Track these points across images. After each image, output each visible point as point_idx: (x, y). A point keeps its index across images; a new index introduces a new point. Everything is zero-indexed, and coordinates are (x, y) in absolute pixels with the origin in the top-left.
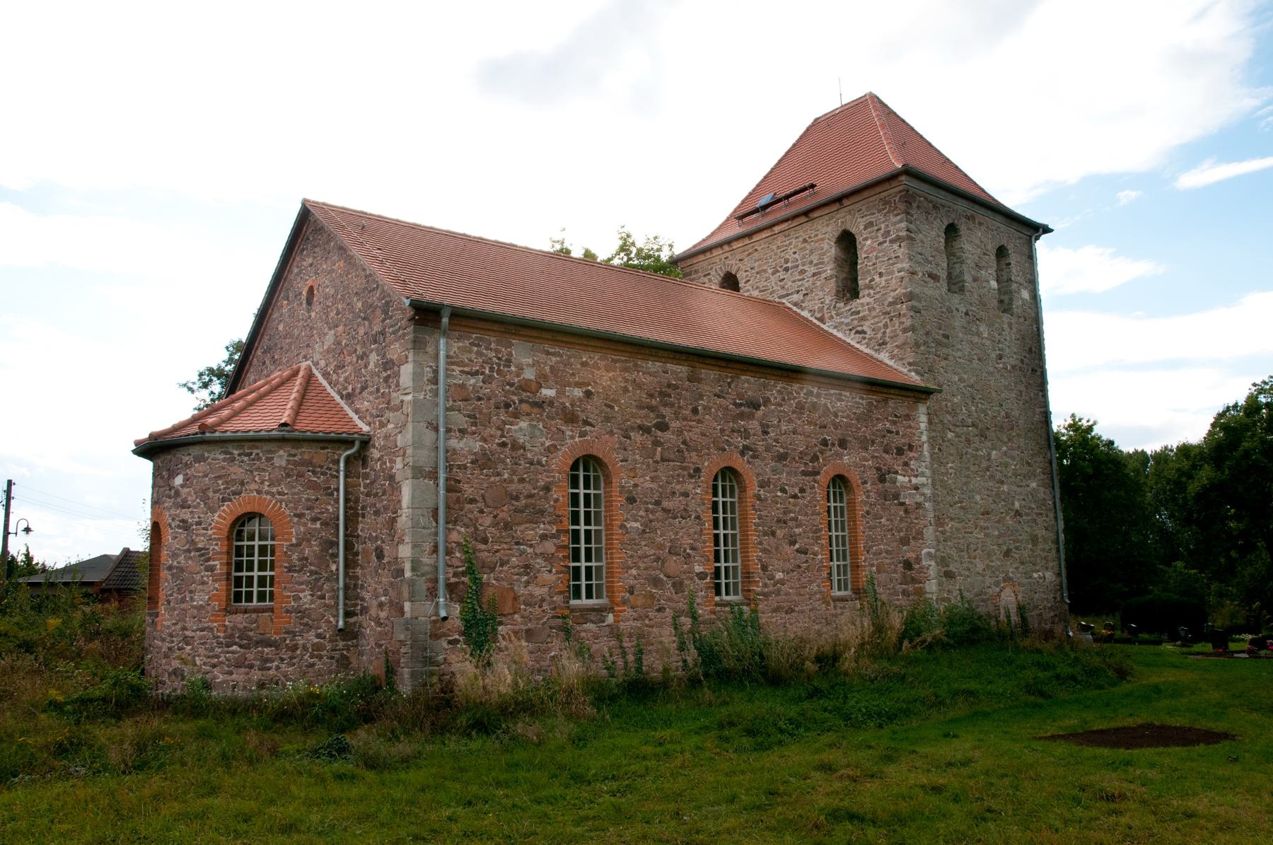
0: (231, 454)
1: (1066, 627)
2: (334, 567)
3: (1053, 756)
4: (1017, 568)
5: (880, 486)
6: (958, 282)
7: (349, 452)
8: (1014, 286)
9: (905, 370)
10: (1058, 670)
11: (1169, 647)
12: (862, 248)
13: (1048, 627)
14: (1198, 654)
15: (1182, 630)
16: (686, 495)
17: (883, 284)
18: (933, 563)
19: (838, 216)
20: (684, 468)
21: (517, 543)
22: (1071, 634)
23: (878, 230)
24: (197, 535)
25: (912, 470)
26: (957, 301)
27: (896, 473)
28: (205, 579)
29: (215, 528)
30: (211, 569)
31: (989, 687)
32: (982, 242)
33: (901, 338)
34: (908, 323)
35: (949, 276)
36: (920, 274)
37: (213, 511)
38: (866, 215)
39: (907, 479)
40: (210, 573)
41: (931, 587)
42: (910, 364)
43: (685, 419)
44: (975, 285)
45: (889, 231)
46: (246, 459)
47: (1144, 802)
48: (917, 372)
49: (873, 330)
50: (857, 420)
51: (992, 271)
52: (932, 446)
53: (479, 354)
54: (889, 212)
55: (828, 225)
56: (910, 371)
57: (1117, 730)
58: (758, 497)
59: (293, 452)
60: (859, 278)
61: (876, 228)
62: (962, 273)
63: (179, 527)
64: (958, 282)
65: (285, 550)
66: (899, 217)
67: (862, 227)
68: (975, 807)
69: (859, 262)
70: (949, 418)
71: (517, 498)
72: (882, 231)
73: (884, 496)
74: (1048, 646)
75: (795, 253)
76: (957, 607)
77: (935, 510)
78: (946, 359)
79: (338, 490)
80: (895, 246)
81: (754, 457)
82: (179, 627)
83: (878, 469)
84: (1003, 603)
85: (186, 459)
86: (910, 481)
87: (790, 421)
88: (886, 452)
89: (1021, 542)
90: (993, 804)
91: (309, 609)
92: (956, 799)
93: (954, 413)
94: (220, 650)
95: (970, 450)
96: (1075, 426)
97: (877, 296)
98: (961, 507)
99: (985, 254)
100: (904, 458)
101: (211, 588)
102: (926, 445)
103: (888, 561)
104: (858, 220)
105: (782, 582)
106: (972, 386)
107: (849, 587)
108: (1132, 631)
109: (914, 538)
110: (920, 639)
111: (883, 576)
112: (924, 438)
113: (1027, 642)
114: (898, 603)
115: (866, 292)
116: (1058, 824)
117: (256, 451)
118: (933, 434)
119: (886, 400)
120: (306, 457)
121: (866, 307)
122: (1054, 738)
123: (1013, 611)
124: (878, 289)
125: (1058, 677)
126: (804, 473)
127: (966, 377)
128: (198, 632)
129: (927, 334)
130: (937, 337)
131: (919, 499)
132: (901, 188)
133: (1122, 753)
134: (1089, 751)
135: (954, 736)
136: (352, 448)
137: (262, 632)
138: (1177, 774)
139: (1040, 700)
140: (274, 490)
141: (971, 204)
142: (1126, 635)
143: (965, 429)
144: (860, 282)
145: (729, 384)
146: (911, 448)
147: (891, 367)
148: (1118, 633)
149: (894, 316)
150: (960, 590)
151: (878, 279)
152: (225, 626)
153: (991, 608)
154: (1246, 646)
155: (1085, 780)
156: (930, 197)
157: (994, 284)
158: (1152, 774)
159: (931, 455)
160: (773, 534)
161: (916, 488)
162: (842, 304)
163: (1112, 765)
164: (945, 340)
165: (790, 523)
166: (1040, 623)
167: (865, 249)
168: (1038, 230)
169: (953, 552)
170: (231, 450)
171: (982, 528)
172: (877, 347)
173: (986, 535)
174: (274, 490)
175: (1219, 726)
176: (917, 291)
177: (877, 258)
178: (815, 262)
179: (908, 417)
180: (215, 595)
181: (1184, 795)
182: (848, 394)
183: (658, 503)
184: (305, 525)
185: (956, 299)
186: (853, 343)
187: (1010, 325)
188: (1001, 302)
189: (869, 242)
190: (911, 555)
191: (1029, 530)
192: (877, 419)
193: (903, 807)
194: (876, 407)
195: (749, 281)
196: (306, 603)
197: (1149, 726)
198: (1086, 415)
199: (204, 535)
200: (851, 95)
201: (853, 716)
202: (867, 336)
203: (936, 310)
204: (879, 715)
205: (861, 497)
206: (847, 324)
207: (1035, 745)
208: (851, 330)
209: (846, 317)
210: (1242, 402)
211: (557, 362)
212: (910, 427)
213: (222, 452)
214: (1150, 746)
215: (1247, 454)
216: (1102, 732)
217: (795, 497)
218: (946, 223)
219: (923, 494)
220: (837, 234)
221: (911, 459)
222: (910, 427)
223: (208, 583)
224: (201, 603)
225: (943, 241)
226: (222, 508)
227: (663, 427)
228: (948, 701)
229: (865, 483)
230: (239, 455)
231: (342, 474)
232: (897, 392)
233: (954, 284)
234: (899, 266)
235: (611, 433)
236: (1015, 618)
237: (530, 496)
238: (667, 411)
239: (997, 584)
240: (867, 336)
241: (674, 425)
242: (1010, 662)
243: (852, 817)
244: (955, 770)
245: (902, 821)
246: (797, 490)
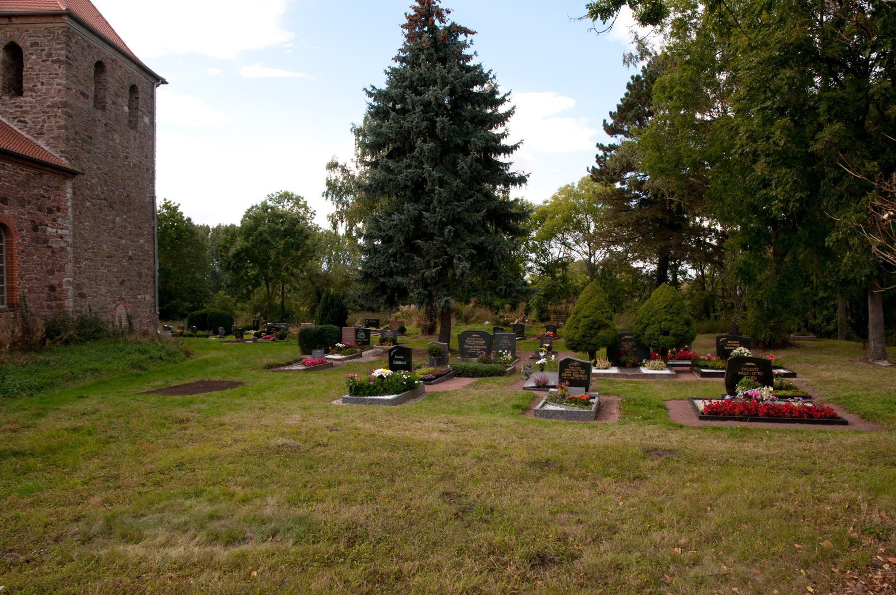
1: (156, 328)
3: (149, 403)
4: (128, 292)
5: (34, 233)
6: (102, 103)
8: (140, 113)
9: (57, 156)
10: (151, 354)
11: (213, 338)
12: (27, 60)
13: (145, 328)
14: (228, 342)
15: (221, 329)
17: (44, 90)
18: (71, 288)
19: (6, 29)
22: (159, 332)
25: (59, 225)
26: (100, 115)
27: (47, 225)
31: (108, 366)
32: (120, 79)
33: (56, 132)
34: (62, 123)
35: (96, 97)
36: (74, 91)
38: (33, 36)
39: (54, 230)
41: (69, 303)
42: (61, 152)
44: (113, 107)
45: (51, 54)
47: (199, 421)
48: (67, 158)
49: (34, 122)
50: (17, 185)
51: (126, 100)
52: (75, 210)
54: (52, 39)
56: (61, 156)
57: (185, 385)
60: (24, 81)
61: (41, 48)
62: (105, 97)
64: (102, 103)
66: (60, 46)
67: (28, 44)
68: (103, 436)
70: (88, 192)
72: (45, 52)
73: (36, 240)
74: (145, 340)
76: (86, 316)
77: (74, 253)
78: (89, 153)
80: (56, 66)
83: (33, 222)
84: (117, 314)
86: (57, 232)
88: (40, 210)
89: (132, 276)
90: (114, 433)
92: (90, 434)
93: (91, 189)
95: (101, 215)
96: (166, 206)
97: (38, 98)
98: (93, 252)
99: (122, 88)
102: (70, 209)
103: (37, 285)
106: (106, 174)
107: (5, 302)
108: (193, 330)
109: (58, 270)
110: (59, 337)
111: (33, 296)
112: (69, 204)
113: (132, 337)
114: (43, 313)
115: (29, 93)
116: (153, 439)
118: (76, 202)
119: (41, 175)
121: (29, 105)
122: (148, 393)
123: (124, 319)
124: (39, 94)
125: (151, 358)
127: (102, 167)
129: (76, 133)
130: (83, 136)
131: (63, 244)
133: (188, 397)
134: (169, 398)
135: (86, 397)
138: (216, 405)
139: (139, 372)
141: (116, 52)
142: (190, 332)
143: (99, 201)
144: (24, 85)
146: (59, 209)
147: (46, 151)
148: (186, 332)
150: (89, 305)
153: (110, 317)
154: (252, 337)
155: (168, 413)
156: (86, 38)
157: (126, 109)
158: (203, 406)
159: (74, 216)
161: (61, 237)
162: (7, 98)
163: (183, 405)
164: (89, 140)
166: (140, 326)
167: (30, 61)
168: (159, 81)
169: (86, 281)
171: (107, 266)
172: (36, 135)
173: (109, 271)
175: (237, 379)
176: (71, 102)
179: (58, 188)
181: (219, 415)
182: (10, 165)
185: (99, 114)
186: (15, 128)
187: (135, 138)
188: (130, 121)
189: (34, 57)
190: (55, 282)
191: (137, 269)
192: (34, 187)
193: (54, 443)
194: (33, 178)
197: (202, 382)
198: (174, 200)
201: (10, 390)
202: (28, 126)
203: (84, 118)
204: (30, 388)
205: (17, 240)
206: (11, 114)
207: (138, 397)
208: (14, 118)
209: (11, 108)
210: (259, 204)
212: (59, 195)
214: (202, 392)
215: (261, 233)
216: (176, 387)
218: (96, 60)
219: (66, 242)
220: (5, 43)
221: (58, 217)
222: (59, 195)
225: (93, 71)
228: (80, 376)
229: (22, 230)
232: (51, 170)
233: (99, 103)
234: (58, 81)
236: (125, 323)
239: (114, 302)
240: (28, 126)
242: (121, 350)
243: (16, 454)
244: (87, 417)
245: (53, 451)
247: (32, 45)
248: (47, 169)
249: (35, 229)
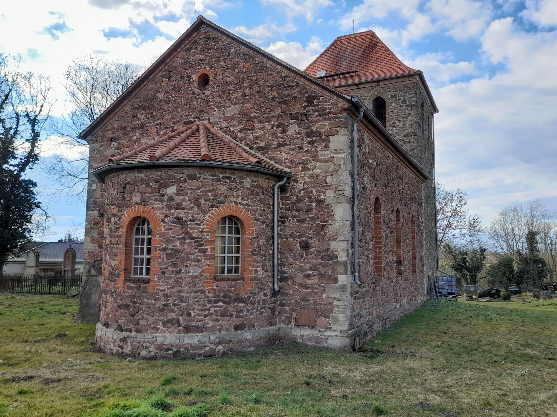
0: (218, 176)
24: (191, 229)
28: (199, 258)
29: (206, 224)
30: (204, 251)
37: (205, 213)
38: (393, 91)
40: (203, 254)
46: (228, 181)
54: (406, 92)
55: (368, 93)
59: (254, 179)
60: (386, 121)
61: (398, 98)
63: (173, 222)
65: (250, 240)
66: (412, 95)
67: (389, 97)
72: (401, 100)
79: (273, 205)
82: (175, 290)
85: (177, 176)
91: (262, 278)
94: (210, 305)
97: (397, 131)
101: (204, 264)
104: (388, 93)
117: (233, 177)
128: (192, 294)
132: (414, 81)
136: (282, 180)
137: (238, 293)
140: (245, 202)
149: (406, 142)
151: (398, 123)
152: (214, 290)
167: (391, 107)
170: (217, 174)
174: (245, 202)
177: (398, 113)
180: (207, 269)
189: (393, 104)
196: (260, 274)
199: (197, 229)
213: (211, 174)
220: (374, 98)
223: (201, 261)
224: (195, 274)
226: (211, 212)
230: (223, 178)
234: (411, 118)
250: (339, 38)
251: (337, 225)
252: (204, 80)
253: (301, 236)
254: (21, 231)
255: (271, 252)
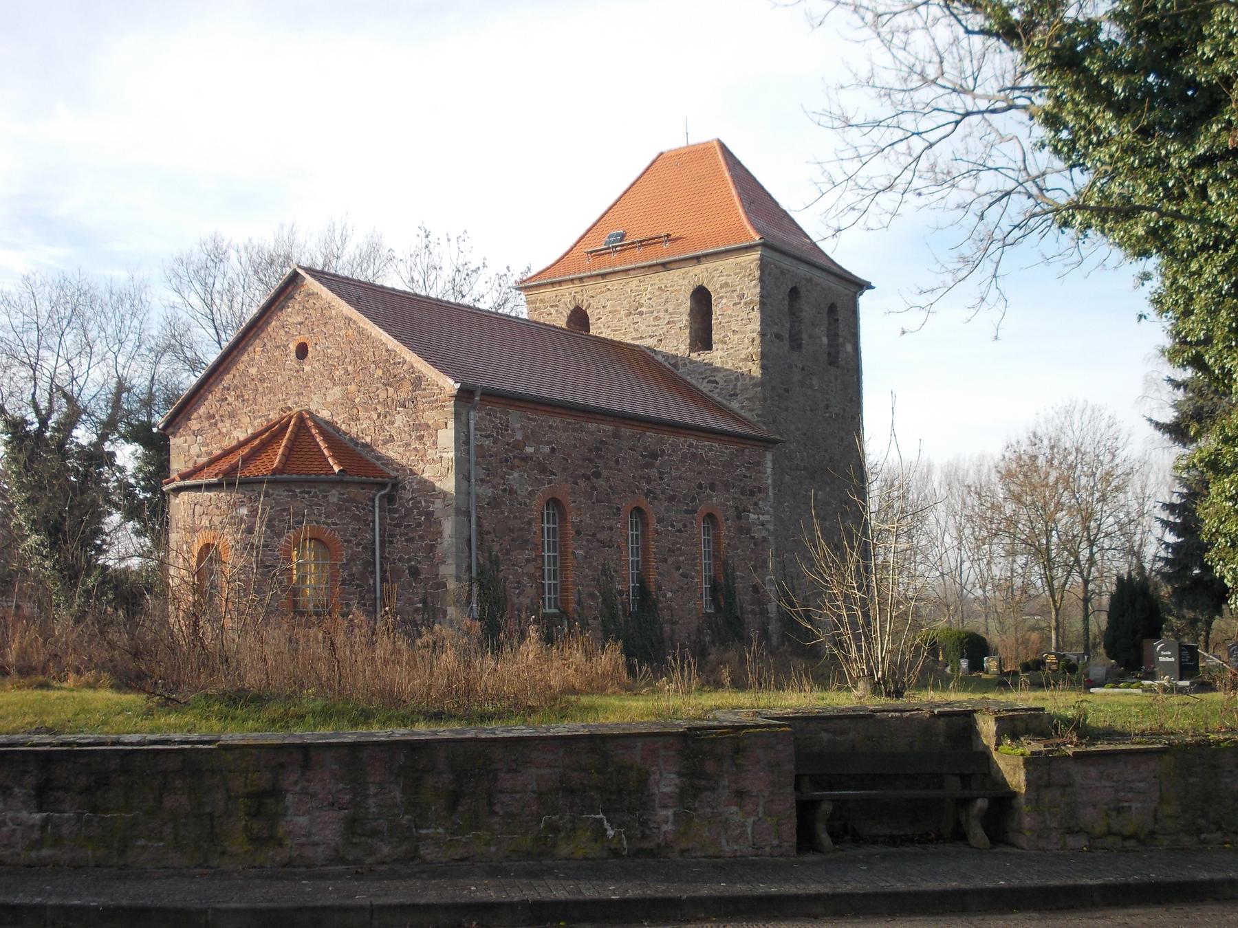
2: (371, 582)
7: (383, 493)
8: (841, 340)
16: (611, 529)
20: (610, 508)
21: (513, 565)
23: (733, 291)
27: (749, 511)
39: (756, 517)
43: (611, 468)
46: (306, 496)
52: (774, 488)
53: (491, 421)
58: (656, 531)
69: (714, 317)
71: (512, 531)
73: (741, 530)
75: (650, 299)
79: (374, 521)
81: (655, 498)
83: (737, 508)
87: (678, 469)
88: (742, 494)
99: (819, 313)
100: (755, 499)
102: (771, 488)
105: (671, 599)
112: (769, 481)
115: (720, 346)
117: (313, 490)
120: (352, 495)
126: (687, 512)
131: (765, 534)
140: (329, 521)
145: (639, 439)
157: (825, 340)
160: (666, 561)
165: (677, 553)
168: (862, 286)
170: (293, 488)
174: (329, 521)
178: (671, 310)
183: (594, 535)
184: (352, 548)
189: (724, 301)
195: (600, 318)
199: (271, 556)
200: (701, 135)
202: (719, 386)
206: (701, 373)
211: (535, 426)
217: (680, 531)
219: (768, 530)
222: (760, 472)
227: (597, 475)
230: (301, 493)
231: (377, 510)
235: (566, 480)
237: (521, 529)
238: (599, 462)
241: (605, 473)
246: (681, 525)
247: (721, 287)
248: (749, 442)
249: (739, 517)
250: (661, 154)
251: (446, 544)
252: (302, 351)
253: (410, 560)
254: (1229, 464)
255: (371, 582)
